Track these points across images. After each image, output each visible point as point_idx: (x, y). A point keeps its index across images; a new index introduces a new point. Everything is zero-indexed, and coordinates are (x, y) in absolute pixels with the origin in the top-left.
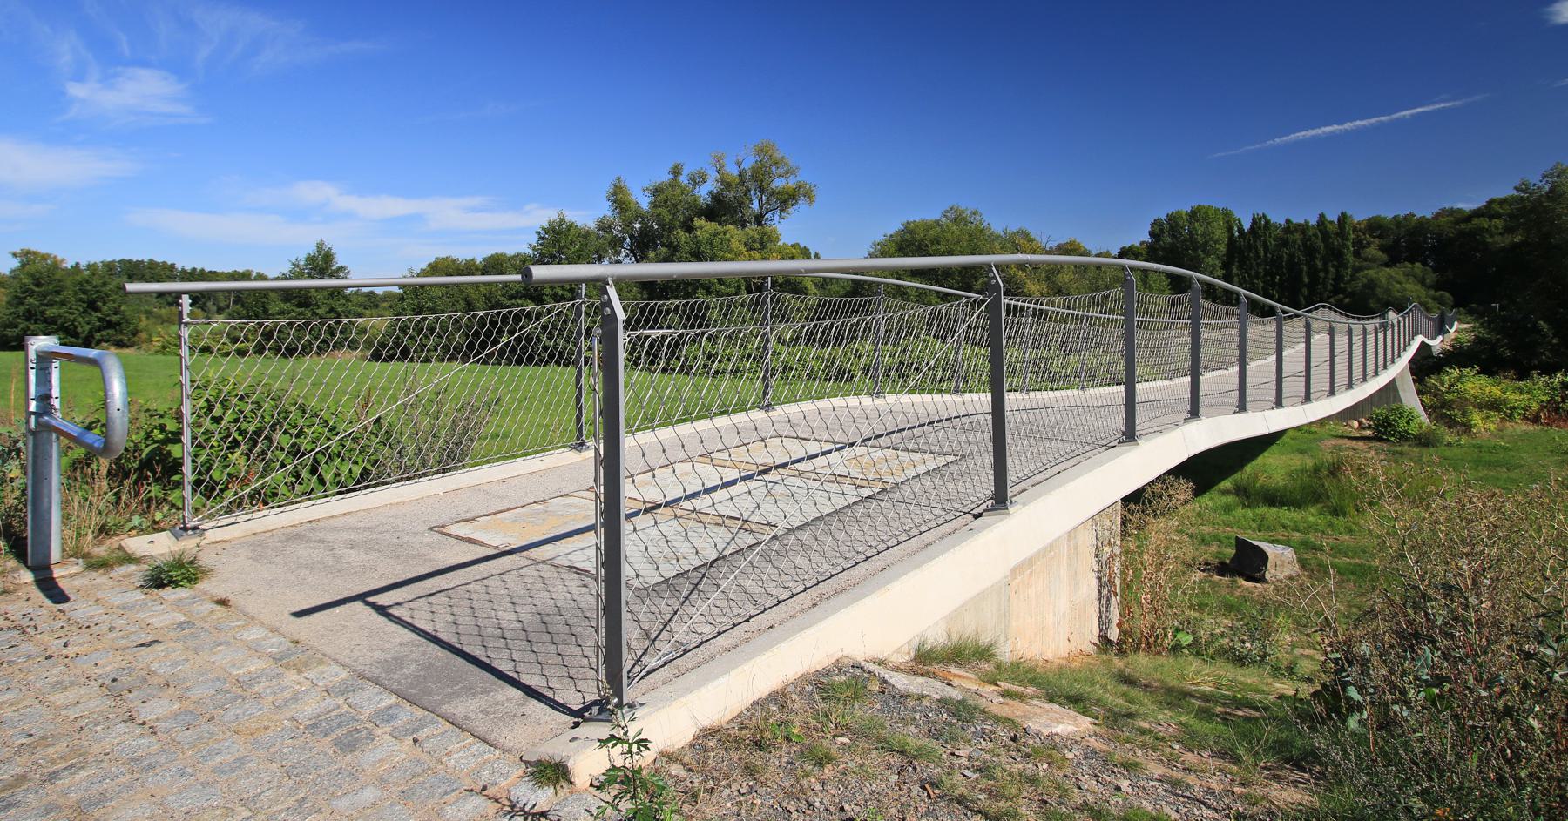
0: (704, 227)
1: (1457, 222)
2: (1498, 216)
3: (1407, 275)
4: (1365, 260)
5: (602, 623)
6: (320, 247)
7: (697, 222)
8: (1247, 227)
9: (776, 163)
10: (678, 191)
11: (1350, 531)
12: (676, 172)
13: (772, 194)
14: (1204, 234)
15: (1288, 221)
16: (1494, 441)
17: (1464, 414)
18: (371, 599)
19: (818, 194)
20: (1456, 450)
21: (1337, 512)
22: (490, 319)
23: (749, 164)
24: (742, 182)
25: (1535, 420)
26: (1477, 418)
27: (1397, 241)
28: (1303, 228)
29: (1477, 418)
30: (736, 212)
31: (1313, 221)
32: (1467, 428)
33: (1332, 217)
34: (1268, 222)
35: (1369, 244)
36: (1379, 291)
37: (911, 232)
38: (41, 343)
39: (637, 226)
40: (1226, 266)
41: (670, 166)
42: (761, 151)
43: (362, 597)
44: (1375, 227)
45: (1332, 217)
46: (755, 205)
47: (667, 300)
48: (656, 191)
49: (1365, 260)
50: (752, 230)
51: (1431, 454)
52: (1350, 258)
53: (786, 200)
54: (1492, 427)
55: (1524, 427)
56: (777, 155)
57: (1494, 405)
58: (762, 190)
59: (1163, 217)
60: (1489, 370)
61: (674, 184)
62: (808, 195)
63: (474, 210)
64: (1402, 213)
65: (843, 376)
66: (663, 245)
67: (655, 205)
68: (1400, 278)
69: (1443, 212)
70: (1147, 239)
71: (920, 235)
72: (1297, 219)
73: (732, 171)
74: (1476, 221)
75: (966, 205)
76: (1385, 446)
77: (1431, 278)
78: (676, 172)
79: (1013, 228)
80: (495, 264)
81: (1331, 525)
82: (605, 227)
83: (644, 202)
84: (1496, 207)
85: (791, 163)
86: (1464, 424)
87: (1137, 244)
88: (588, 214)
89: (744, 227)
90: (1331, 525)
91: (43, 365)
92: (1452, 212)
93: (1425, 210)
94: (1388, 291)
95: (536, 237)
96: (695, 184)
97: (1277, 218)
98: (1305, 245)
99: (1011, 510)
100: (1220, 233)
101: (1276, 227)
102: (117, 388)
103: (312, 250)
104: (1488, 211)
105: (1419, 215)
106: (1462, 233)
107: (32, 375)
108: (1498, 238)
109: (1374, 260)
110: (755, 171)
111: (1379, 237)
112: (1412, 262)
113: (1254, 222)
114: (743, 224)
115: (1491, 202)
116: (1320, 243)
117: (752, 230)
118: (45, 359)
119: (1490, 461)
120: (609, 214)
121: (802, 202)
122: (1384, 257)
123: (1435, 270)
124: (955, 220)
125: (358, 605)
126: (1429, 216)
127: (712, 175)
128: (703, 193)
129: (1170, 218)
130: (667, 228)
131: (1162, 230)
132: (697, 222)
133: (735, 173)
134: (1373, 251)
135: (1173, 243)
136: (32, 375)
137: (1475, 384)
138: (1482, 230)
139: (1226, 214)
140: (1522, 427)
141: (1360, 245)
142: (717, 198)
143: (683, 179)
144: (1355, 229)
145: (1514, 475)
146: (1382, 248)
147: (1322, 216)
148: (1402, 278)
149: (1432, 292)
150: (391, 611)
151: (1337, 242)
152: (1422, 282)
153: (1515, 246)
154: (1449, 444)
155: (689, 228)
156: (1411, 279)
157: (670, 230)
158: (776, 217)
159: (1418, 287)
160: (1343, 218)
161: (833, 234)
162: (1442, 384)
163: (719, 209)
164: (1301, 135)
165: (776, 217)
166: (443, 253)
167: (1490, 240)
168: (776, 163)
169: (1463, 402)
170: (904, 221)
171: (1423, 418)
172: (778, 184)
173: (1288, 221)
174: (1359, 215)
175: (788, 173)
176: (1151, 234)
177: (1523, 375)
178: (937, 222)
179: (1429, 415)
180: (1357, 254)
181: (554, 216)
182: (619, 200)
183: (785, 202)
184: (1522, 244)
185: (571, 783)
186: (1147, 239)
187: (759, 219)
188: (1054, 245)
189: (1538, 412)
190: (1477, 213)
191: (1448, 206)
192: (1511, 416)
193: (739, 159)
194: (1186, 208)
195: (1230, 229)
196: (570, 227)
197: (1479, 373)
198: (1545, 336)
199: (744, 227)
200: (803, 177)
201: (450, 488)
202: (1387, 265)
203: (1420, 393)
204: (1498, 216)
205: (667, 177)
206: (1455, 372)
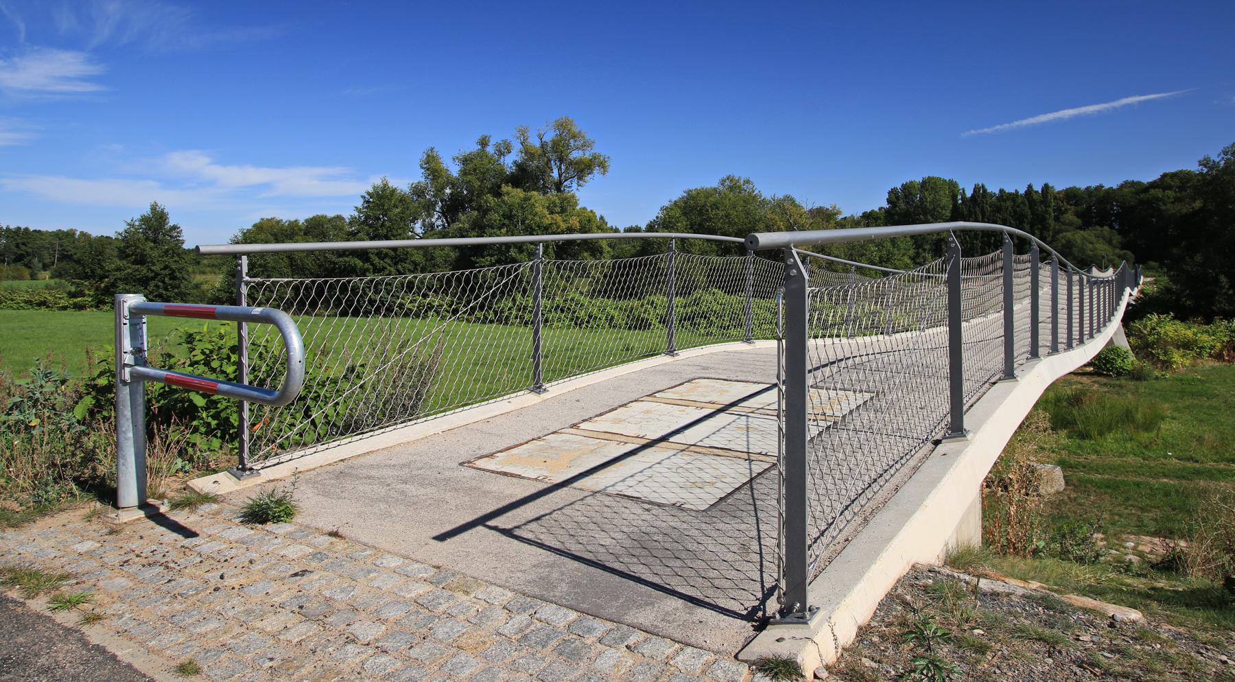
0: (514, 194)
1: (1137, 193)
2: (1169, 187)
3: (1097, 237)
4: (1064, 224)
5: (783, 541)
6: (154, 208)
7: (505, 188)
8: (969, 194)
9: (574, 137)
10: (486, 161)
11: (1097, 452)
12: (484, 143)
13: (571, 164)
14: (932, 202)
15: (1001, 191)
16: (1190, 375)
17: (1165, 354)
18: (491, 523)
19: (612, 165)
20: (1163, 383)
21: (1084, 436)
22: (325, 272)
23: (549, 137)
24: (545, 153)
25: (1219, 357)
26: (1177, 357)
27: (1089, 208)
28: (1014, 197)
29: (1177, 357)
30: (538, 181)
31: (1022, 191)
32: (1167, 365)
33: (1038, 188)
34: (985, 191)
35: (1066, 210)
36: (1075, 250)
37: (693, 198)
38: (132, 300)
39: (448, 191)
40: (1032, 227)
41: (478, 137)
42: (562, 126)
43: (482, 521)
44: (1071, 195)
45: (1038, 188)
46: (555, 174)
47: (480, 259)
48: (466, 161)
49: (1064, 224)
50: (552, 194)
51: (1143, 386)
52: (1051, 222)
53: (582, 170)
54: (1187, 363)
55: (1211, 363)
56: (575, 130)
57: (1186, 345)
58: (561, 160)
59: (899, 186)
60: (1183, 315)
61: (482, 154)
62: (603, 166)
63: (333, 178)
64: (1094, 185)
65: (641, 324)
66: (473, 209)
67: (464, 173)
68: (1092, 240)
69: (1126, 184)
70: (886, 205)
71: (701, 201)
72: (1010, 189)
73: (535, 143)
74: (1152, 191)
75: (740, 174)
76: (1103, 380)
77: (1117, 239)
78: (484, 143)
79: (780, 196)
80: (317, 228)
81: (1080, 447)
82: (418, 191)
83: (455, 170)
84: (1168, 180)
85: (587, 137)
86: (1164, 362)
87: (876, 209)
88: (405, 179)
89: (545, 193)
90: (1080, 447)
91: (135, 321)
92: (1133, 184)
93: (1112, 182)
94: (1082, 250)
95: (362, 201)
96: (501, 154)
97: (993, 188)
98: (1015, 212)
99: (969, 436)
100: (946, 201)
101: (992, 195)
102: (296, 342)
103: (146, 211)
104: (1164, 182)
105: (1107, 186)
106: (1141, 202)
107: (126, 331)
108: (1169, 206)
109: (1071, 224)
110: (555, 144)
111: (1076, 204)
112: (1102, 226)
113: (976, 189)
114: (544, 190)
115: (1165, 176)
116: (1027, 210)
117: (552, 194)
118: (136, 313)
119: (1188, 389)
120: (423, 180)
121: (597, 170)
122: (1079, 222)
123: (1120, 232)
124: (731, 188)
125: (480, 528)
126: (1115, 187)
127: (517, 147)
128: (509, 162)
129: (904, 187)
130: (476, 194)
131: (897, 198)
132: (505, 188)
133: (538, 144)
134: (1070, 217)
135: (905, 205)
136: (126, 331)
137: (1172, 328)
138: (1158, 199)
139: (952, 185)
140: (1209, 363)
141: (1060, 212)
142: (521, 167)
143: (490, 150)
144: (1055, 198)
145: (1214, 402)
146: (1077, 214)
147: (1030, 187)
148: (1093, 239)
149: (1117, 251)
150: (517, 532)
151: (1041, 208)
152: (1110, 242)
153: (1195, 213)
154: (1157, 378)
155: (497, 193)
156: (1101, 240)
157: (479, 196)
158: (575, 185)
159: (1106, 247)
160: (1046, 188)
161: (623, 199)
162: (1145, 327)
163: (524, 177)
164: (1031, 121)
165: (575, 185)
166: (268, 214)
167: (1163, 207)
168: (574, 137)
169: (1162, 343)
170: (686, 189)
171: (1132, 357)
172: (575, 155)
173: (1001, 191)
174: (1059, 186)
175: (585, 146)
176: (889, 201)
177: (1208, 321)
178: (715, 189)
179: (1137, 354)
180: (1057, 219)
181: (378, 182)
182: (432, 166)
183: (582, 171)
184: (1201, 210)
185: (802, 676)
186: (886, 205)
187: (558, 186)
188: (858, 213)
189: (1221, 351)
190: (1153, 185)
191: (1130, 179)
192: (1200, 354)
193: (542, 133)
194: (918, 179)
195: (954, 197)
196: (394, 191)
197: (1174, 318)
198: (1222, 288)
199: (545, 193)
200: (598, 149)
201: (446, 427)
202: (1080, 228)
203: (1128, 336)
204: (1169, 187)
205: (475, 148)
206: (1155, 317)
